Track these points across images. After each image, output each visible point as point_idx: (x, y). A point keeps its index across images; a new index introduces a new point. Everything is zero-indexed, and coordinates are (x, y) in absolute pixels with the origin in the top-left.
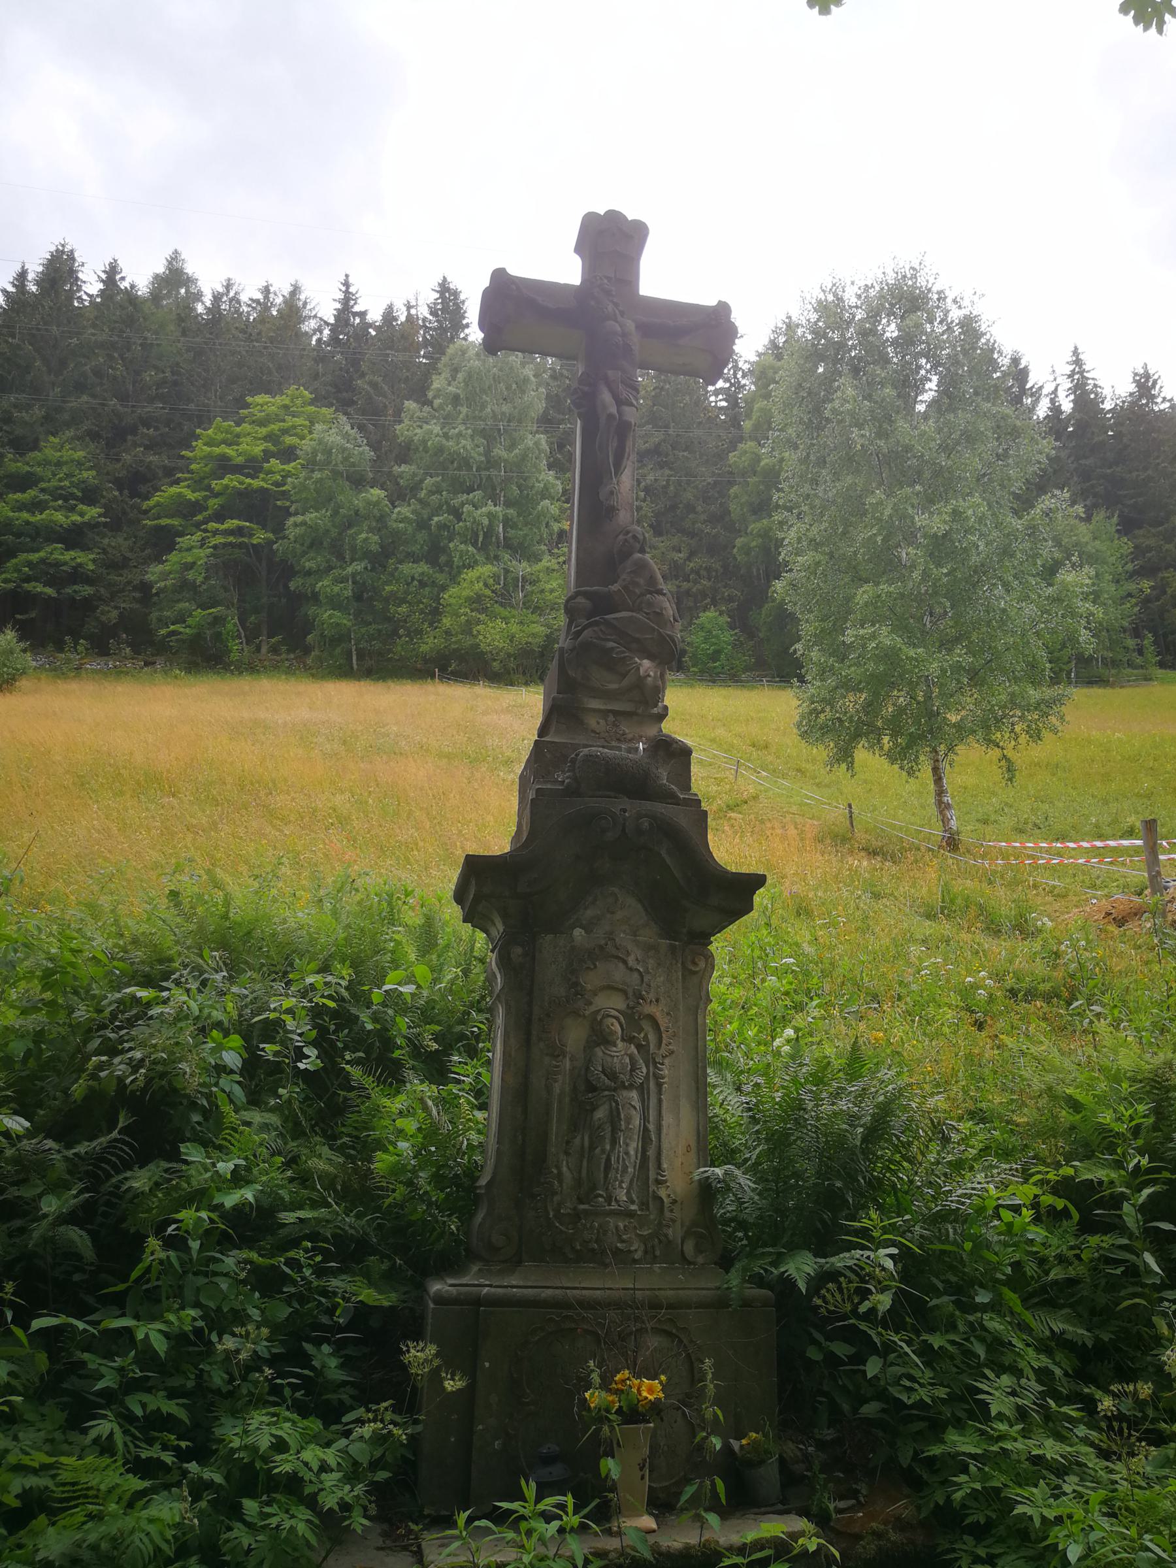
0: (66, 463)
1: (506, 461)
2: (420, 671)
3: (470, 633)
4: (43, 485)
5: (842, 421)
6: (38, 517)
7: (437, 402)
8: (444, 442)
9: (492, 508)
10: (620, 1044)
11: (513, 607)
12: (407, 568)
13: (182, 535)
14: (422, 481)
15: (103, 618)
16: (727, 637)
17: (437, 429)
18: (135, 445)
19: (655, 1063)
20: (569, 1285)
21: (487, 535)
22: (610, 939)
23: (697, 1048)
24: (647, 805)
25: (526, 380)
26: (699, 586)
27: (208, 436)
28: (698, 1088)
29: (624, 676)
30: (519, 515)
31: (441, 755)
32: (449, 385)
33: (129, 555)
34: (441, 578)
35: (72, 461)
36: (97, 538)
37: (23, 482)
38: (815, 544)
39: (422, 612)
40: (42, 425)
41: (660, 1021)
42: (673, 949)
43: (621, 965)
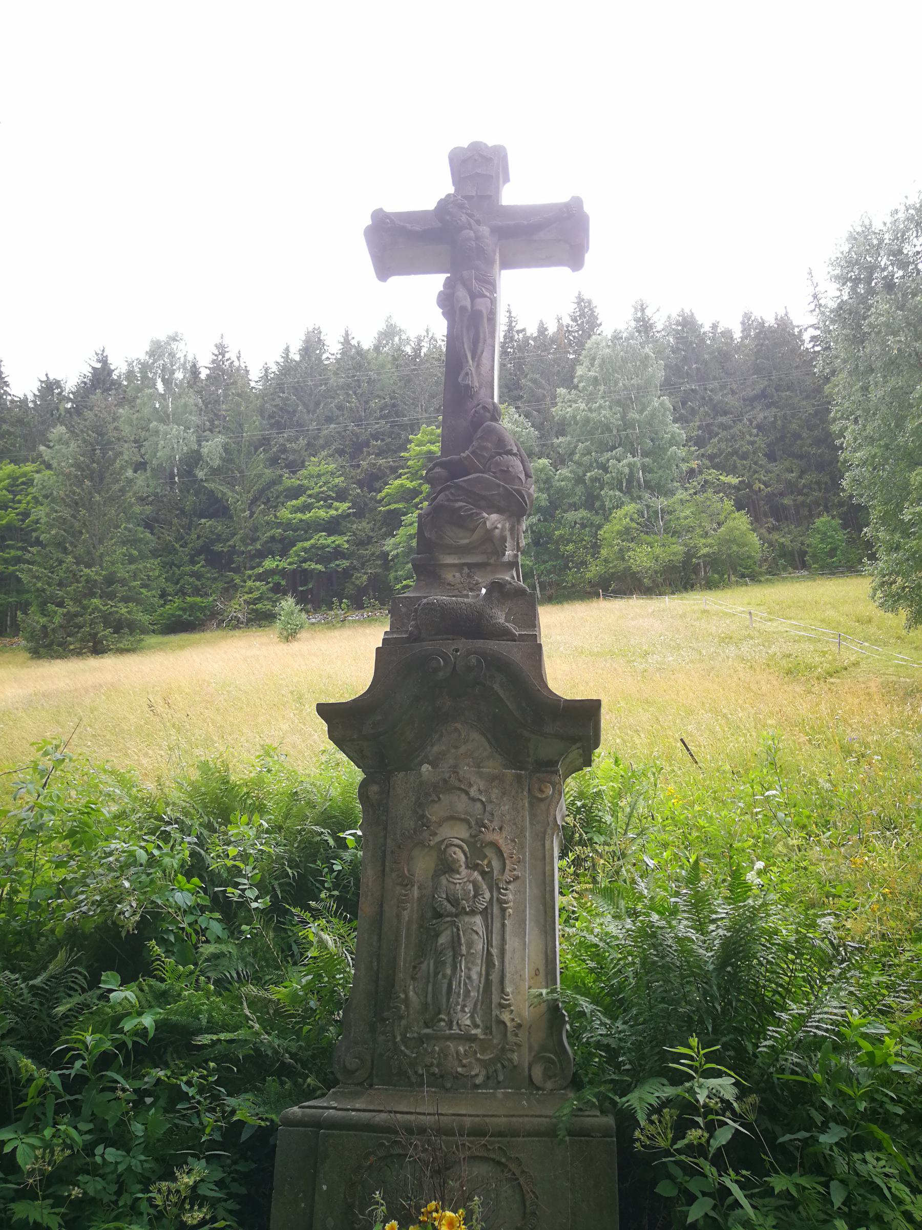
0: (324, 474)
1: (638, 421)
2: (589, 593)
3: (623, 559)
4: (309, 492)
5: (879, 332)
6: (307, 516)
7: (581, 385)
8: (589, 414)
9: (632, 459)
10: (464, 871)
11: (656, 534)
12: (571, 516)
13: (405, 514)
14: (576, 447)
15: (357, 582)
17: (583, 406)
18: (369, 454)
19: (499, 889)
20: (405, 1110)
21: (630, 481)
23: (545, 873)
24: (480, 643)
25: (647, 357)
26: (811, 498)
27: (418, 439)
28: (546, 912)
29: (474, 530)
30: (654, 461)
31: (592, 654)
32: (589, 371)
33: (371, 534)
34: (597, 520)
35: (327, 472)
36: (349, 525)
37: (296, 492)
38: (871, 440)
39: (585, 547)
40: (306, 450)
42: (519, 778)
43: (464, 797)
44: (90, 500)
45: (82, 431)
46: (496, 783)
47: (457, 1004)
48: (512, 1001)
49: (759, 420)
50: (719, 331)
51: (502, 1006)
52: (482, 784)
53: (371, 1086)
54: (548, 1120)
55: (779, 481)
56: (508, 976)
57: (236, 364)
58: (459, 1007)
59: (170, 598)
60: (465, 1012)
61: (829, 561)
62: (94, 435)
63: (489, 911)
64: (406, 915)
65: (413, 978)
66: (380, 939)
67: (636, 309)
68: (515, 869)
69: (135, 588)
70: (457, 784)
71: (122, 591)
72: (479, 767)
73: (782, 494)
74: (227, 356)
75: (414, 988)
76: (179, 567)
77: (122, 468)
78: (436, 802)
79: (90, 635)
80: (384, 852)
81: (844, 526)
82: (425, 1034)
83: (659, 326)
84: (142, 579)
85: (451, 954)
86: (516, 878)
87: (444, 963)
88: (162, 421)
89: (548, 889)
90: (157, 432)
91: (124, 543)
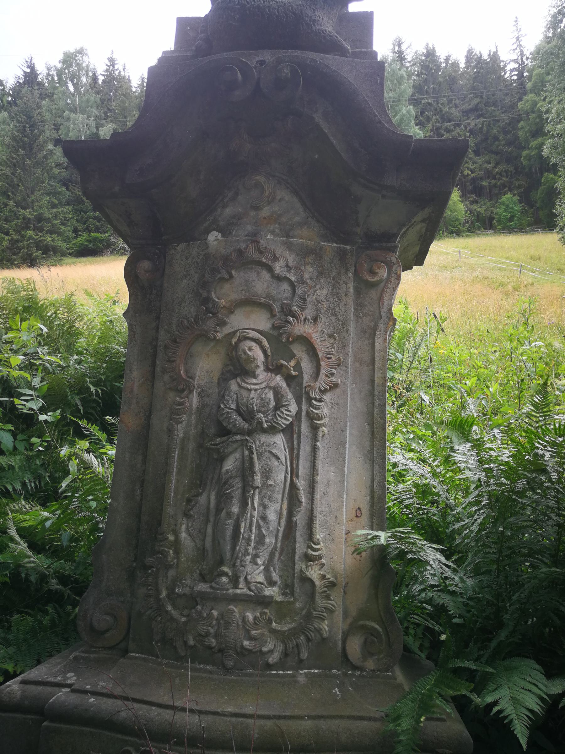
10: (262, 374)
16: (518, 207)
19: (309, 399)
22: (253, 242)
23: (372, 381)
25: (402, 77)
28: (373, 433)
41: (318, 345)
42: (342, 255)
43: (265, 274)
44: (24, 163)
45: (16, 114)
46: (310, 259)
47: (246, 553)
48: (323, 552)
49: (471, 127)
50: (450, 62)
51: (308, 558)
52: (291, 259)
53: (126, 652)
54: (377, 725)
55: (480, 169)
56: (319, 517)
57: (122, 73)
58: (249, 558)
59: (80, 233)
60: (256, 564)
61: (508, 224)
62: (24, 117)
63: (295, 428)
64: (180, 431)
65: (187, 515)
66: (144, 462)
67: (394, 45)
68: (332, 374)
69: (56, 224)
70: (256, 256)
71: (48, 226)
72: (288, 236)
73: (481, 179)
74: (116, 67)
75: (187, 528)
76: (85, 213)
77: (45, 142)
78: (227, 280)
79: (27, 254)
80: (155, 348)
81: (520, 202)
82: (199, 592)
83: (409, 58)
84: (61, 219)
85: (240, 485)
86: (335, 386)
87: (229, 497)
88: (71, 111)
89: (377, 402)
90: (69, 119)
91: (48, 194)
